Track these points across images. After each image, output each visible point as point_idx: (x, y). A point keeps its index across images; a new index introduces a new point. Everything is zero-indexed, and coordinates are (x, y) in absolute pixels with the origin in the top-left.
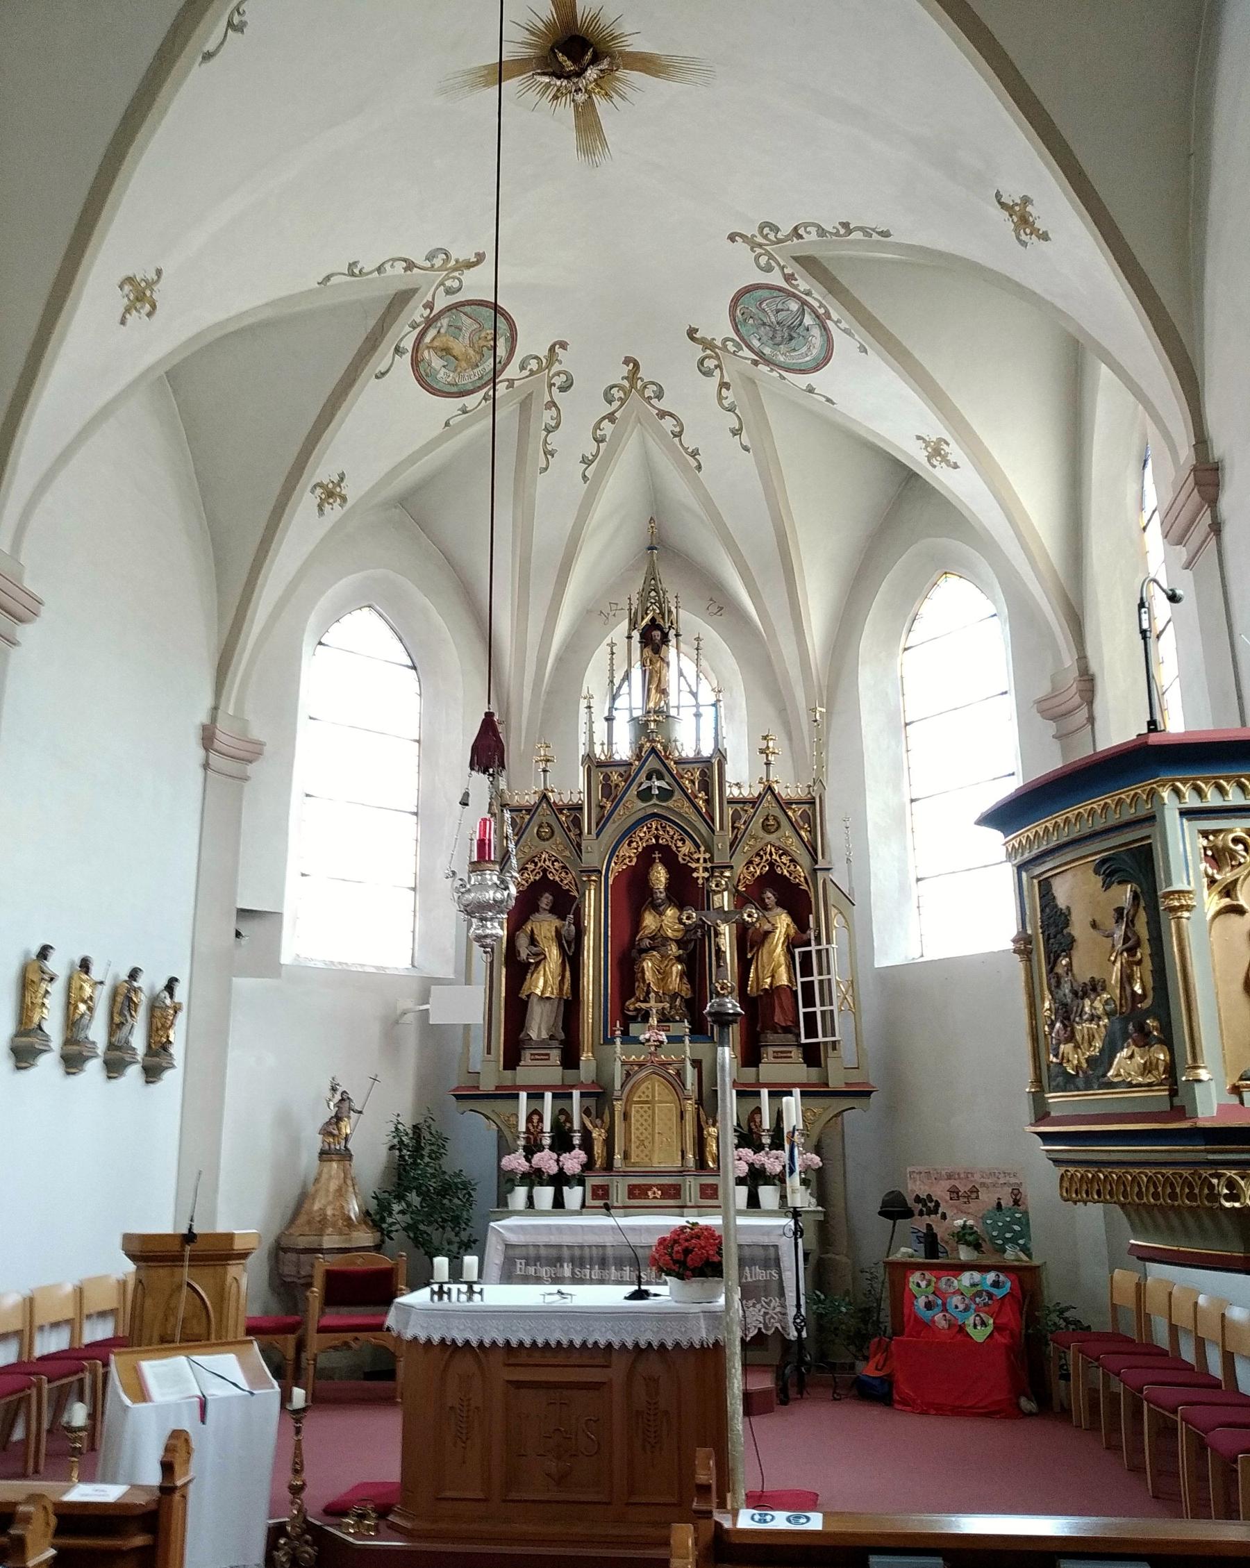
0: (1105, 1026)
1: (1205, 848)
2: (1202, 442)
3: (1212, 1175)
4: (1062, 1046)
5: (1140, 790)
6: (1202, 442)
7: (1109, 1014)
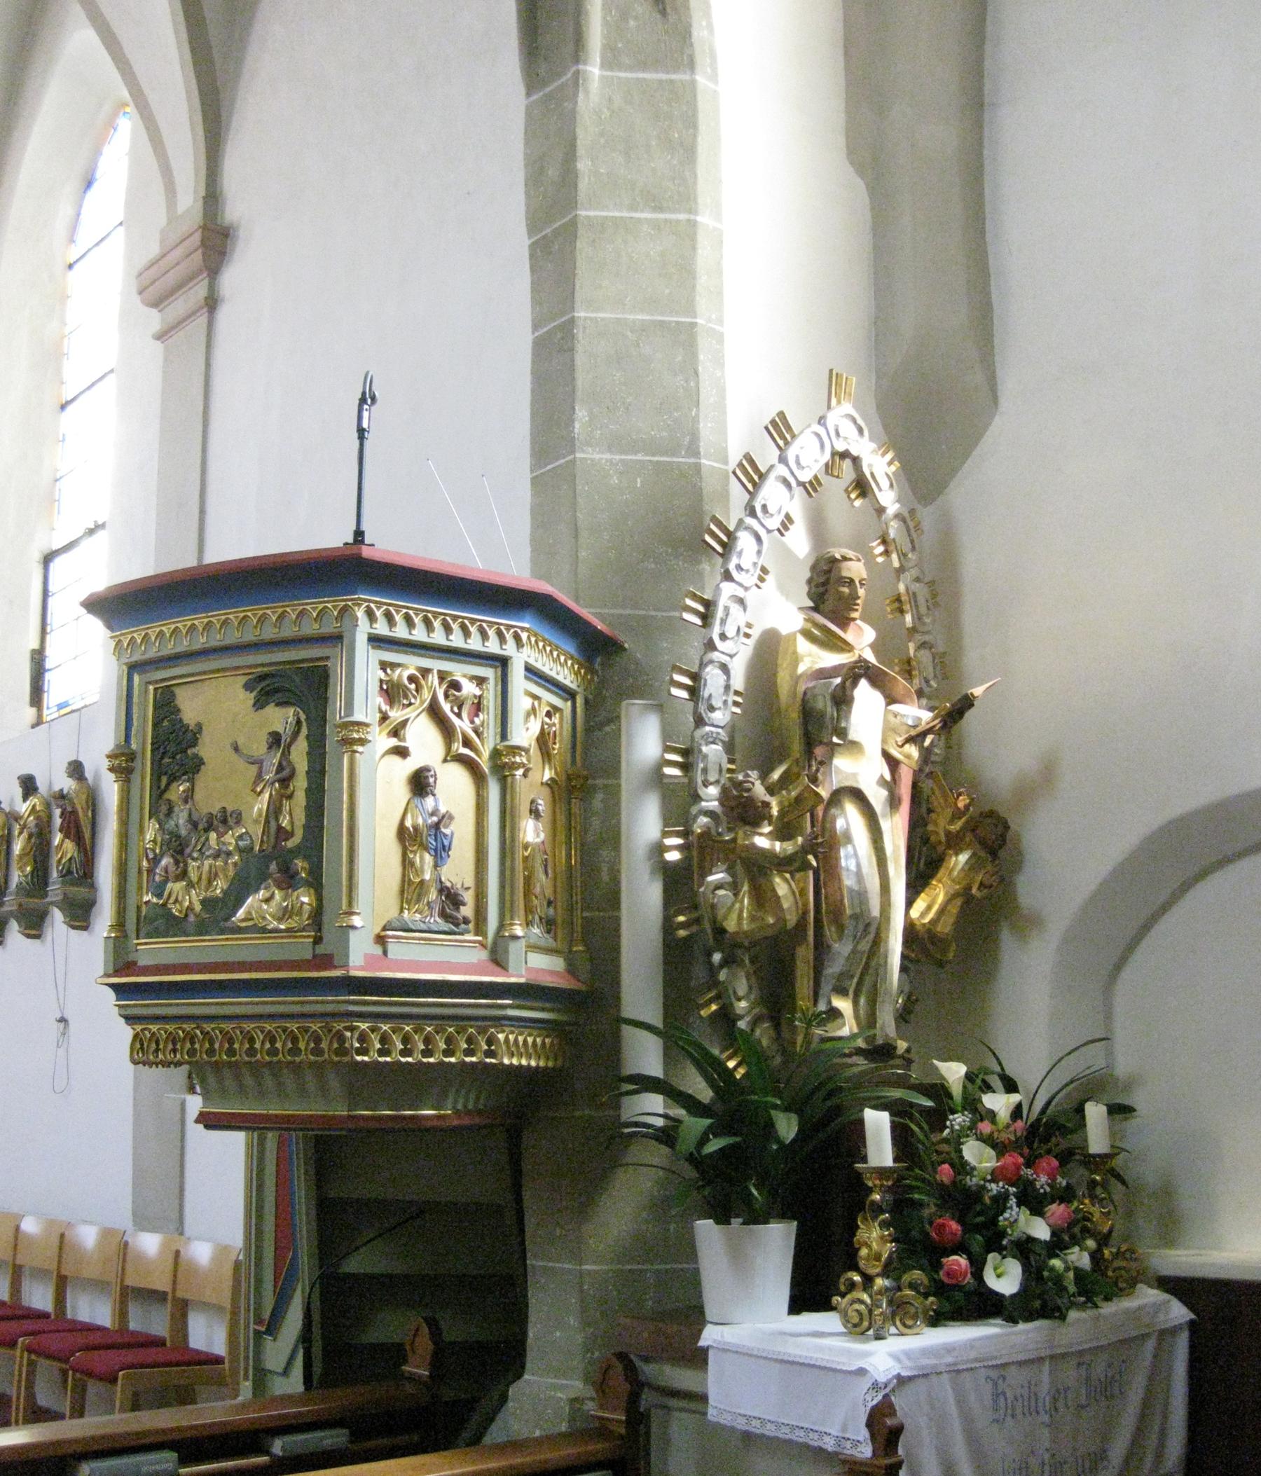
0: (235, 864)
1: (381, 681)
2: (212, 197)
3: (347, 1029)
4: (170, 885)
5: (331, 604)
6: (212, 197)
7: (240, 851)
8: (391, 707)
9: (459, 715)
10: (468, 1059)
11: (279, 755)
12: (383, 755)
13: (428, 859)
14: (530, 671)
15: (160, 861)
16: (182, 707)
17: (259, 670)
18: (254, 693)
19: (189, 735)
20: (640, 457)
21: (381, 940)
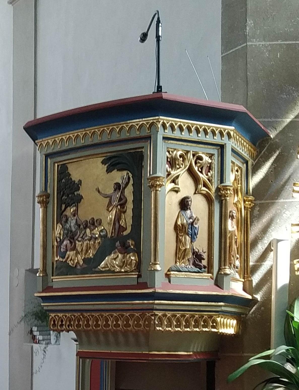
0: (99, 243)
3: (152, 315)
4: (68, 253)
8: (172, 169)
9: (201, 172)
10: (204, 329)
11: (119, 194)
12: (168, 192)
13: (188, 238)
14: (233, 151)
15: (63, 242)
16: (71, 173)
17: (109, 154)
18: (106, 166)
19: (76, 186)
20: (279, 42)
21: (168, 276)
